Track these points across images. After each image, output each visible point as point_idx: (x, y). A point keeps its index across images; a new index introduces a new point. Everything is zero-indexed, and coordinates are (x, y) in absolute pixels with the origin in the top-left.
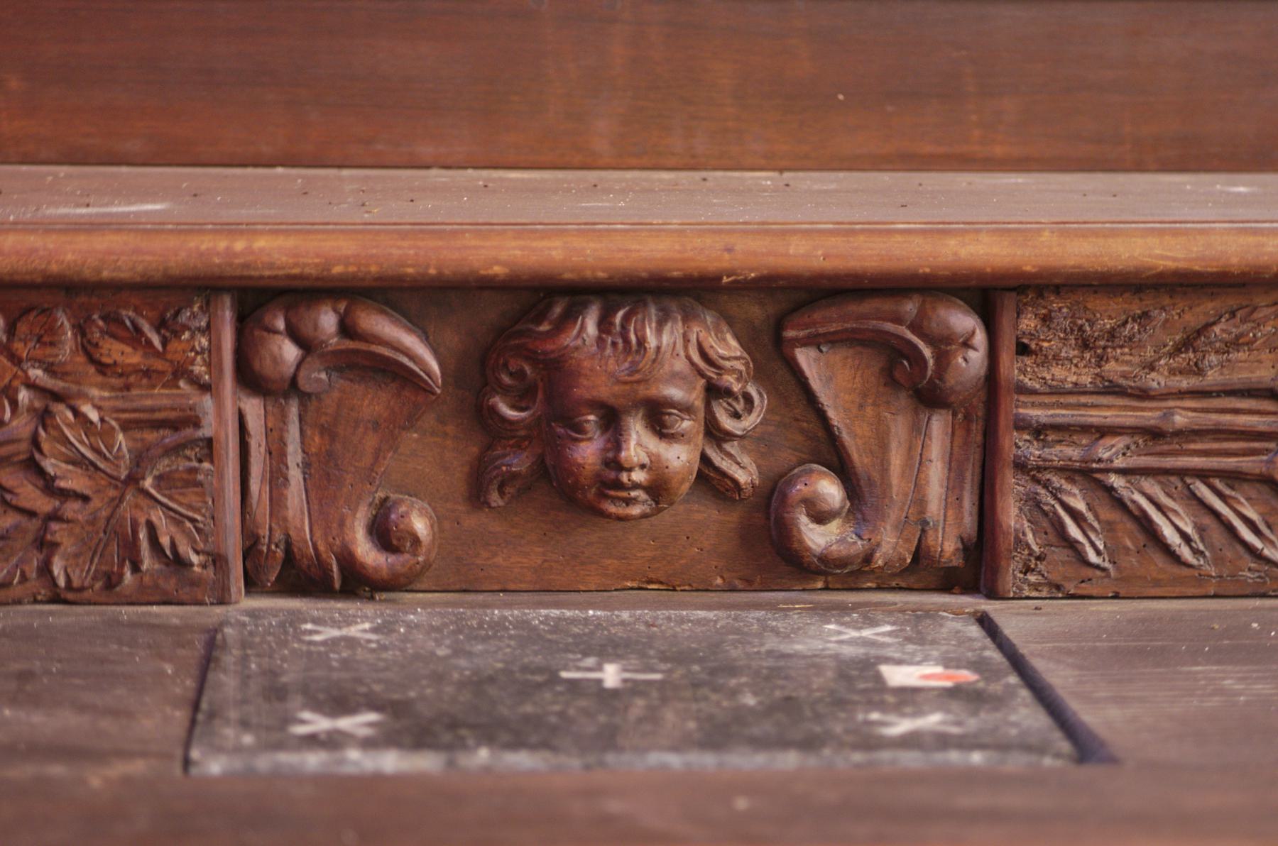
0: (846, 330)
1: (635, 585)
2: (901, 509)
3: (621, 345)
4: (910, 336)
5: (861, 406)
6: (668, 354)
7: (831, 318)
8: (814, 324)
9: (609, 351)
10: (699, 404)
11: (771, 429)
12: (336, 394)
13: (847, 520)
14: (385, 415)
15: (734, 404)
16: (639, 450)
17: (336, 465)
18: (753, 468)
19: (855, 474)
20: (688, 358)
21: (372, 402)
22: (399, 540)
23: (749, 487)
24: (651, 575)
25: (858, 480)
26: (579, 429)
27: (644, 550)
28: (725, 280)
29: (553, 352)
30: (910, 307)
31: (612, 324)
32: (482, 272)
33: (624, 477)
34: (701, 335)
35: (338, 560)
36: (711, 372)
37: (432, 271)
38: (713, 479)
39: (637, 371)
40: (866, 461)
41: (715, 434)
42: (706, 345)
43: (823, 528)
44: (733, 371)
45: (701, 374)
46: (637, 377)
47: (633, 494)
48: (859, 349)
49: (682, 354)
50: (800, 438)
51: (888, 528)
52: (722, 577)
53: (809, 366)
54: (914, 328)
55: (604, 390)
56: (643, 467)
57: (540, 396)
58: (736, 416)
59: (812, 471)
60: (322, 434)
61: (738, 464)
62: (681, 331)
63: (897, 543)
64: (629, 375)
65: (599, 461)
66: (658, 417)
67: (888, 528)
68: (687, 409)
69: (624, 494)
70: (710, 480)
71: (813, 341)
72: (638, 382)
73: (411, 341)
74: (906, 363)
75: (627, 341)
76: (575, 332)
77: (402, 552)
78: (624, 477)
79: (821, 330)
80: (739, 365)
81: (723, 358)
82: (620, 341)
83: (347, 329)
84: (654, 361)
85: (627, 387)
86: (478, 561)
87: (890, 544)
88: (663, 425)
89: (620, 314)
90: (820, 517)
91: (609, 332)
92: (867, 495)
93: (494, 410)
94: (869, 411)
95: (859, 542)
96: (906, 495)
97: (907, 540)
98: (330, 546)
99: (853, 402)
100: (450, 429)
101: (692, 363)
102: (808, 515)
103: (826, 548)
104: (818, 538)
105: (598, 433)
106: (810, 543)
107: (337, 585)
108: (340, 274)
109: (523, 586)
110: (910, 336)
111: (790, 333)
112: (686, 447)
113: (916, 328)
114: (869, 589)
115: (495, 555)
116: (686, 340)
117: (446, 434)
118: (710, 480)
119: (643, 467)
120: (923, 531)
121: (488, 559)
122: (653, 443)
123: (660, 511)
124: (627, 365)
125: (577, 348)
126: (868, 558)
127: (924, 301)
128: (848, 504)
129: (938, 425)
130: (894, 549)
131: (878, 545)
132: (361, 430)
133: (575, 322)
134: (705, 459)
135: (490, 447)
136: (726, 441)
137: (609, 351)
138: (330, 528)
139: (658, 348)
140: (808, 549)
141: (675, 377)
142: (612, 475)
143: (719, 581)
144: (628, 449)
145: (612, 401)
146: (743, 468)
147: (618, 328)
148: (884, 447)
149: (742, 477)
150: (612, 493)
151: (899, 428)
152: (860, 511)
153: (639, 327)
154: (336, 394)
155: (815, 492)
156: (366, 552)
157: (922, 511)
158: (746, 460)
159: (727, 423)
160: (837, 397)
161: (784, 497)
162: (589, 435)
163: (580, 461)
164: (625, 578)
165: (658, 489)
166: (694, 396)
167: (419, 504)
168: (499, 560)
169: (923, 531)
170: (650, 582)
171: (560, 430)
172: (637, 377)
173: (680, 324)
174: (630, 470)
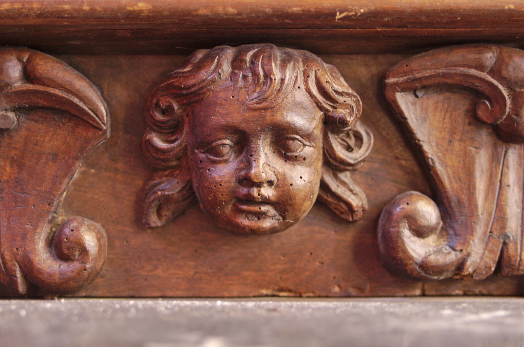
0: (438, 75)
1: (269, 292)
2: (487, 225)
3: (250, 78)
4: (490, 79)
5: (450, 142)
6: (291, 86)
7: (425, 66)
8: (412, 71)
9: (241, 83)
10: (318, 133)
11: (376, 165)
12: (23, 133)
13: (441, 236)
14: (63, 148)
15: (347, 140)
16: (267, 168)
17: (22, 189)
18: (363, 196)
19: (447, 197)
20: (308, 91)
21: (52, 137)
22: (69, 249)
23: (360, 210)
24: (282, 285)
25: (450, 202)
26: (216, 152)
27: (276, 264)
28: (339, 16)
29: (194, 85)
30: (489, 57)
31: (243, 61)
32: (129, 8)
33: (255, 192)
34: (319, 73)
35: (21, 267)
36: (327, 105)
37: (86, 8)
38: (330, 203)
39: (265, 99)
40: (456, 186)
41: (332, 163)
42: (323, 80)
43: (422, 240)
44: (345, 105)
45: (321, 108)
46: (264, 104)
47: (264, 208)
48: (448, 94)
49: (303, 87)
50: (399, 173)
51: (476, 241)
52: (339, 286)
53: (408, 108)
54: (492, 72)
55: (236, 117)
56: (270, 183)
57: (186, 129)
58: (349, 149)
59: (411, 195)
60: (12, 164)
61: (351, 191)
62: (302, 69)
63: (483, 254)
64: (257, 103)
65: (234, 180)
66: (283, 140)
67: (476, 241)
68: (308, 136)
69: (255, 208)
70: (328, 204)
71: (413, 88)
72: (265, 109)
73: (82, 85)
74: (487, 103)
75: (255, 74)
76: (212, 68)
77: (73, 260)
78: (255, 192)
79: (418, 76)
80: (349, 101)
81: (337, 92)
82: (250, 75)
83: (28, 75)
84: (279, 91)
85: (256, 114)
86: (143, 273)
87: (478, 255)
88: (288, 149)
89: (251, 53)
90: (420, 232)
91: (241, 68)
92: (457, 214)
93: (149, 143)
94: (457, 144)
95: (453, 253)
96: (490, 214)
97: (492, 251)
98: (15, 255)
99: (443, 139)
100: (120, 165)
101: (312, 96)
102: (410, 229)
103: (426, 258)
104: (417, 248)
105: (233, 155)
106: (412, 253)
107: (21, 288)
108: (8, 10)
109: (179, 293)
110: (490, 79)
111: (391, 80)
112: (308, 169)
113: (495, 72)
114: (457, 296)
115: (156, 267)
116: (306, 76)
117: (116, 170)
118: (328, 204)
119: (270, 183)
120: (505, 244)
121: (150, 271)
122: (280, 165)
123: (287, 226)
124: (256, 95)
125: (213, 81)
126: (460, 266)
127: (501, 53)
128: (441, 223)
129: (513, 155)
130: (482, 258)
131: (469, 255)
132: (43, 161)
133: (213, 61)
134: (324, 186)
135: (150, 178)
136: (342, 171)
137: (241, 83)
138: (15, 240)
139: (283, 80)
140: (411, 258)
141: (297, 105)
142: (244, 191)
143: (337, 289)
144: (258, 166)
145: (243, 126)
146: (355, 194)
147: (248, 65)
148: (470, 174)
149: (355, 202)
150: (245, 207)
151: (482, 160)
152: (453, 228)
153: (265, 62)
154: (23, 133)
155: (415, 210)
156: (45, 261)
157: (503, 227)
158: (357, 189)
159: (341, 152)
160: (430, 134)
161: (390, 214)
162: (225, 158)
163: (218, 179)
164: (261, 287)
165: (284, 205)
166: (314, 125)
167: (87, 222)
168: (159, 272)
169: (505, 244)
170: (281, 290)
171: (202, 156)
172: (264, 104)
173: (301, 64)
174: (259, 185)
